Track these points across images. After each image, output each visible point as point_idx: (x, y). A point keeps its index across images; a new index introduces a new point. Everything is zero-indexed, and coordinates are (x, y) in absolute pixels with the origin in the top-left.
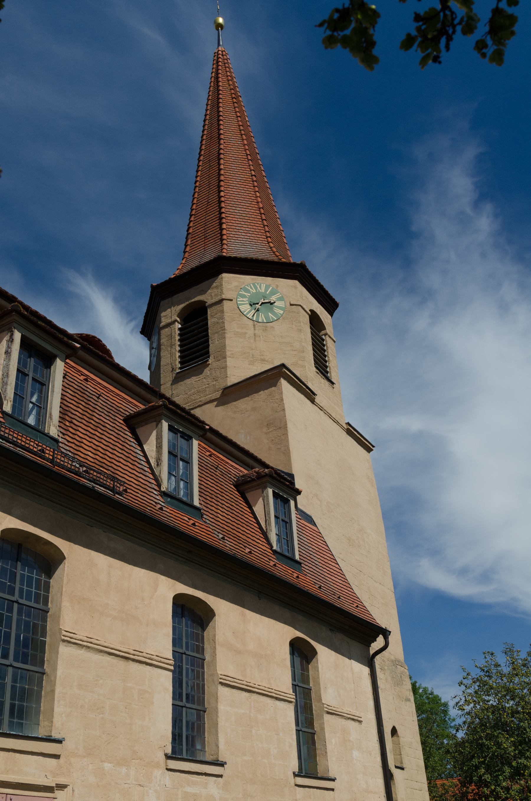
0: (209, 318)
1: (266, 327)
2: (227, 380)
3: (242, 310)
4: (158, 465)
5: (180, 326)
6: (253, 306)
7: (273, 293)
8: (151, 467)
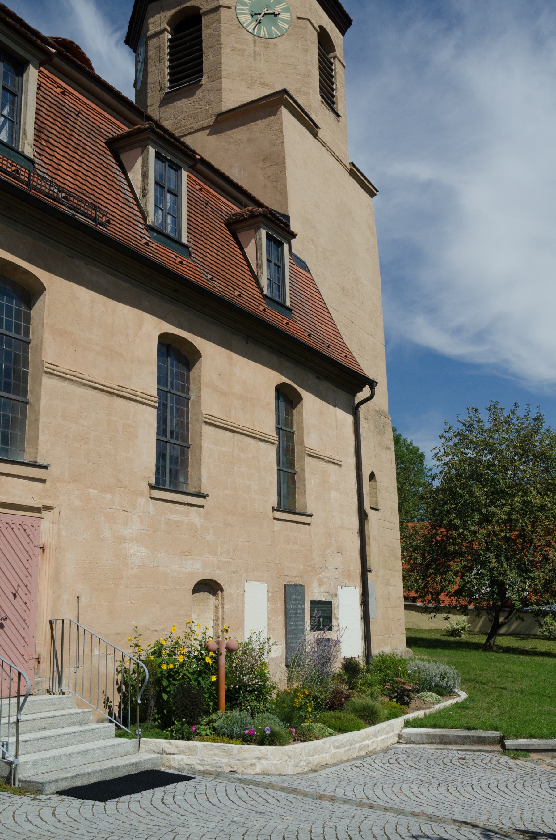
0: (203, 28)
1: (268, 44)
2: (221, 104)
3: (241, 21)
4: (143, 196)
5: (170, 37)
8: (136, 198)
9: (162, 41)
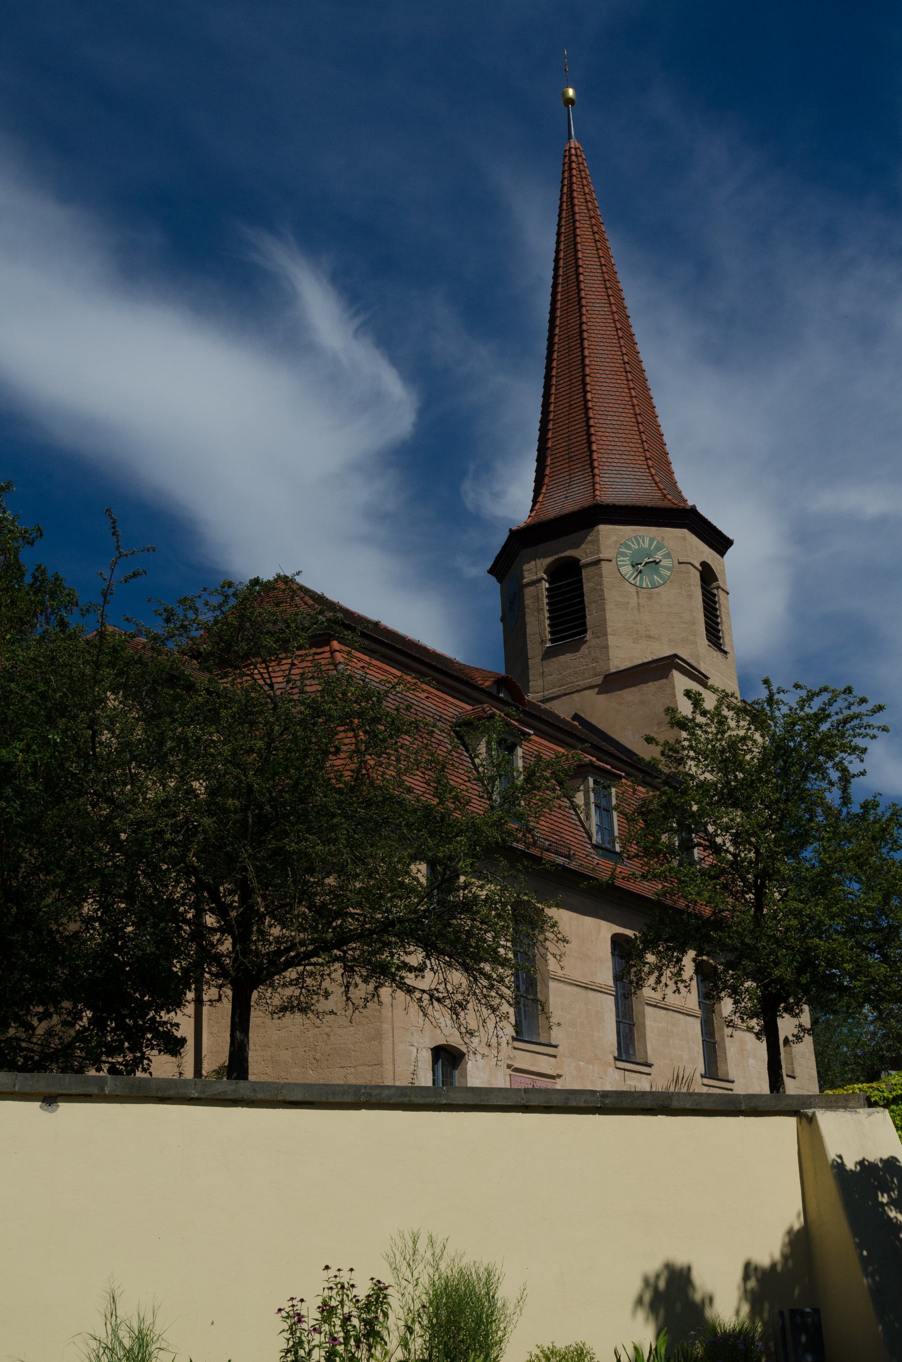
0: (584, 581)
1: (652, 594)
4: (587, 819)
7: (659, 548)
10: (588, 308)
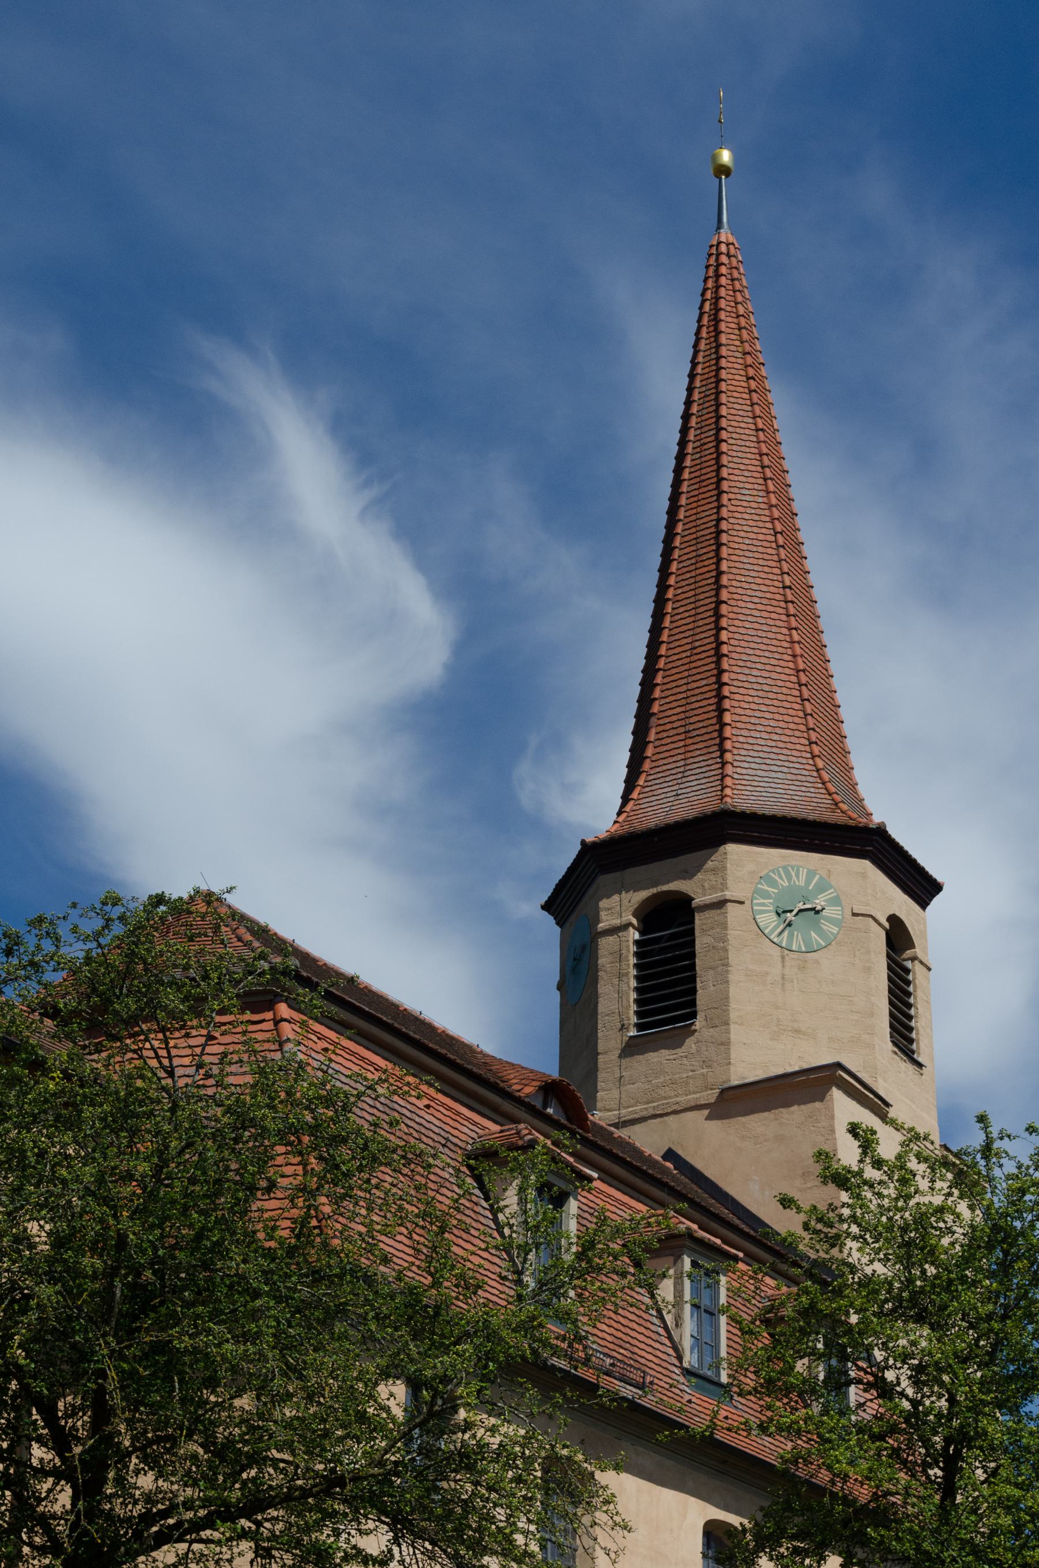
0: (697, 933)
2: (729, 1069)
3: (761, 924)
4: (677, 1325)
5: (637, 936)
6: (783, 915)
7: (821, 888)
8: (666, 1328)
9: (624, 944)
10: (731, 496)
